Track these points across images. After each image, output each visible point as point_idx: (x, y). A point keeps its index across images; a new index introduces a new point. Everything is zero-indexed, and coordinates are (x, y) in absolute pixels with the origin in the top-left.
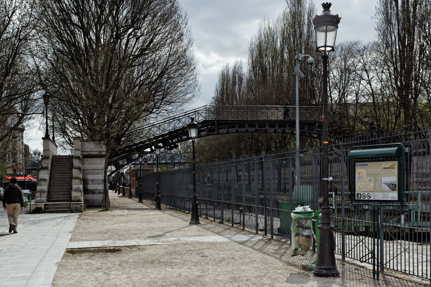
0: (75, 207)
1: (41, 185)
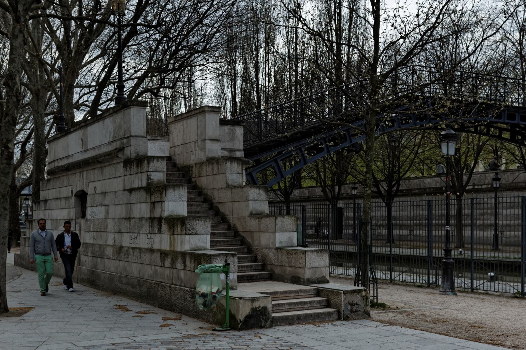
0: (351, 301)
1: (196, 234)
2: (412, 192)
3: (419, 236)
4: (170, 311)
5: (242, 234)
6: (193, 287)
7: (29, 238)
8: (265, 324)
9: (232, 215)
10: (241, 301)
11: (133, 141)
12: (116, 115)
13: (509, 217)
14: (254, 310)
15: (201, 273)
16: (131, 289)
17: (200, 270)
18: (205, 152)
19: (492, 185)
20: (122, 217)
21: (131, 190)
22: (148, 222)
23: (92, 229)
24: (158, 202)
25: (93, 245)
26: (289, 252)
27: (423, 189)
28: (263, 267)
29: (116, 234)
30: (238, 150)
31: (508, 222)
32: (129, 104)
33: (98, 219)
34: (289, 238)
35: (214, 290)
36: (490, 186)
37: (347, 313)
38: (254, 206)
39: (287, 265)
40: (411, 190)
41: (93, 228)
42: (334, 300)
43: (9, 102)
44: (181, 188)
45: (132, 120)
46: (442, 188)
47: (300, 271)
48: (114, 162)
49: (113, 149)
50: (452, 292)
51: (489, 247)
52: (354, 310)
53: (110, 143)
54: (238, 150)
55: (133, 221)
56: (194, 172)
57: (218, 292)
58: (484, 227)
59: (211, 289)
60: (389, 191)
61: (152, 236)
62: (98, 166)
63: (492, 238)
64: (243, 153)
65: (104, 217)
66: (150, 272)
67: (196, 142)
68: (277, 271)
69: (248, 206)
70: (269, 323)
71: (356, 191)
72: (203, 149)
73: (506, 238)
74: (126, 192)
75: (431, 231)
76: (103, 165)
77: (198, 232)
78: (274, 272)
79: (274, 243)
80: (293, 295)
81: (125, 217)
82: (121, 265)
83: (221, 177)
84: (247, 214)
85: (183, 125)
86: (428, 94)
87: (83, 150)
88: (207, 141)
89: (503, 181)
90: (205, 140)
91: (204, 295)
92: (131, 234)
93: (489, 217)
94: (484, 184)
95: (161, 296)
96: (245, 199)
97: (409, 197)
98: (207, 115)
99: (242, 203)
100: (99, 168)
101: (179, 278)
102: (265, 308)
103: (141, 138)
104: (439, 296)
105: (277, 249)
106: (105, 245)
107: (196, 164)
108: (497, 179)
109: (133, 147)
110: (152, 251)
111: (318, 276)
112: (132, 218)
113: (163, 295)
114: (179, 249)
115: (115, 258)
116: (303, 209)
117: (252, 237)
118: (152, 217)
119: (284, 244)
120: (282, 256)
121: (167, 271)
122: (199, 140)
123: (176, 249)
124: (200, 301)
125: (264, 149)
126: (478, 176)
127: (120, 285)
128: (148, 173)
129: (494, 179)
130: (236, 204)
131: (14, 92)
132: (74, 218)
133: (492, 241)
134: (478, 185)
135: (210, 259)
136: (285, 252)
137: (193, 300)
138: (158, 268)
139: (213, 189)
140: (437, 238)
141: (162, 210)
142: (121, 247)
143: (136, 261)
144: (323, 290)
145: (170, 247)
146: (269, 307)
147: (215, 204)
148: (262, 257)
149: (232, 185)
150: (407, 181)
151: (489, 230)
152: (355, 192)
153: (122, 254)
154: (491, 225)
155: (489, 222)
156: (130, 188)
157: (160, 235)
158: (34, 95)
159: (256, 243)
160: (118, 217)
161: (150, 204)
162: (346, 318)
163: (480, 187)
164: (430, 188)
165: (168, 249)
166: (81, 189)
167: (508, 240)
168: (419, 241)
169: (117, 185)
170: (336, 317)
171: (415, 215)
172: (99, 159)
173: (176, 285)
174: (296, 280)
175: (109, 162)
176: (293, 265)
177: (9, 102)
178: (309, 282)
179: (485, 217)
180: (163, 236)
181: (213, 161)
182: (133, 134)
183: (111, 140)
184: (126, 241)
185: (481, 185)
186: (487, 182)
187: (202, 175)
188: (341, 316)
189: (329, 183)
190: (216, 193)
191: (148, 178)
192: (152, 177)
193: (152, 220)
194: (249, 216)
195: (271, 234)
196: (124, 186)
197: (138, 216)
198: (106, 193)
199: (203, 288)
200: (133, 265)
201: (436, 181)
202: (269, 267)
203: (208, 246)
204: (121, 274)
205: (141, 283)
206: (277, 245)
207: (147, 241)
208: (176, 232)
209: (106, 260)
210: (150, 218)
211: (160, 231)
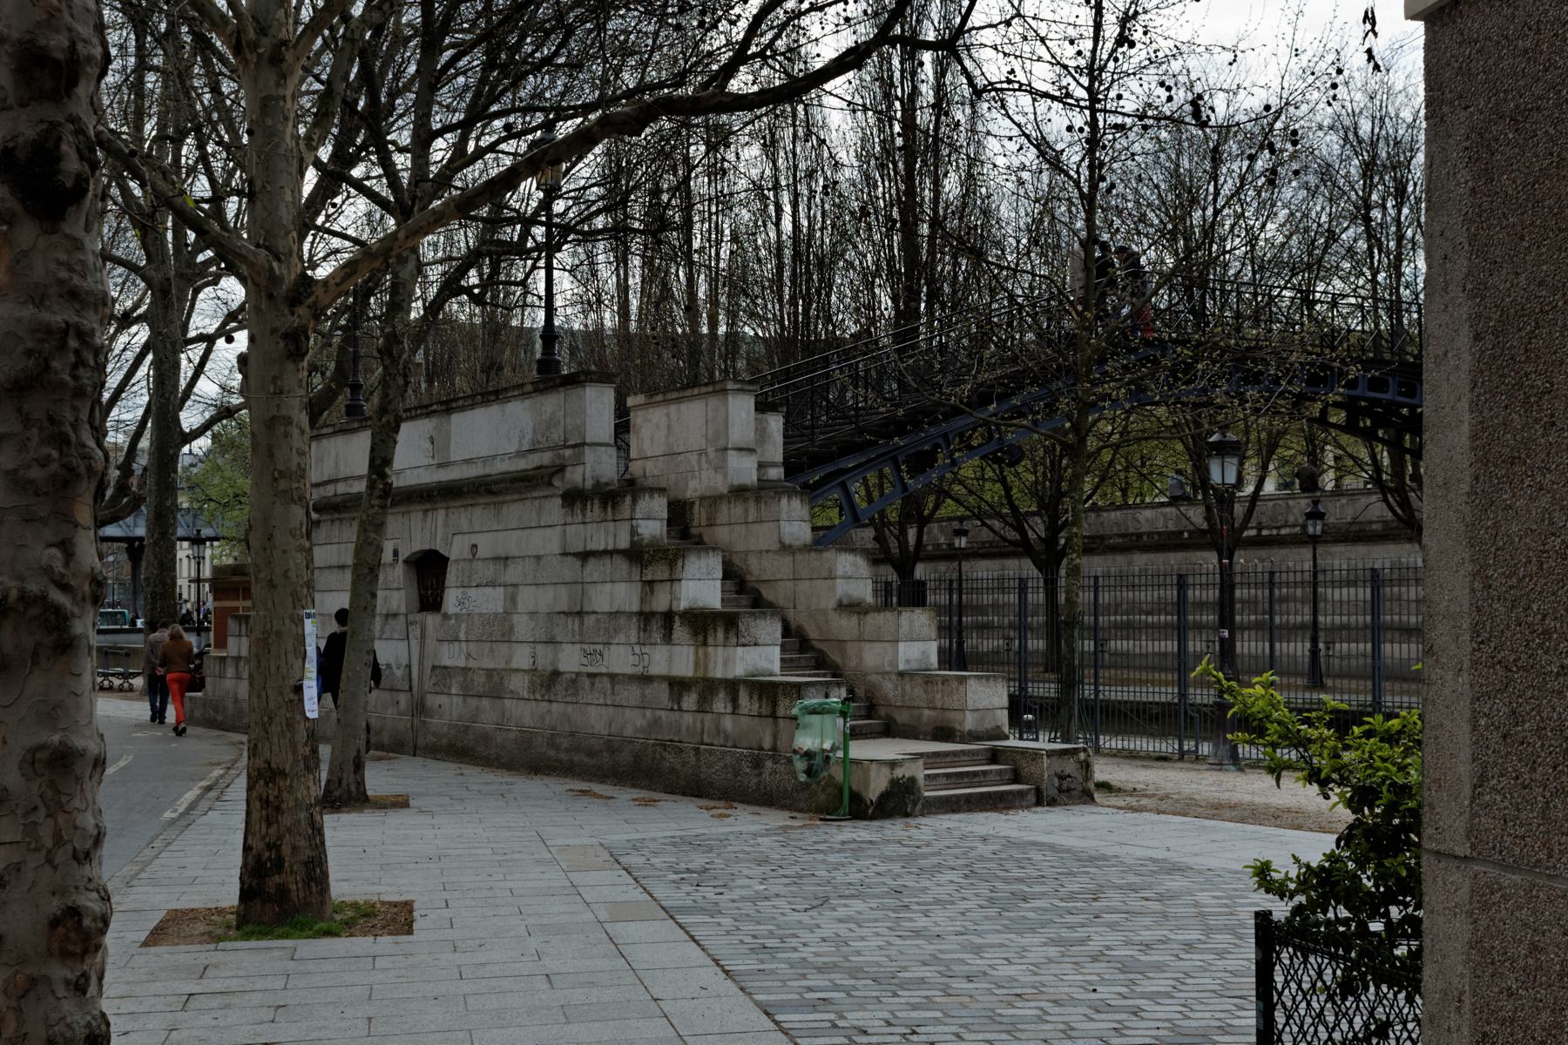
1: (756, 645)
2: (1106, 542)
3: (1127, 654)
4: (696, 796)
5: (818, 645)
6: (754, 745)
7: (238, 659)
8: (913, 810)
9: (795, 607)
10: (874, 766)
11: (589, 455)
12: (540, 398)
13: (1345, 606)
14: (894, 783)
15: (804, 714)
16: (586, 760)
17: (801, 709)
18: (725, 475)
19: (1304, 527)
20: (558, 610)
21: (585, 556)
22: (635, 620)
23: (462, 636)
24: (662, 581)
25: (466, 670)
26: (929, 680)
27: (1132, 534)
28: (871, 710)
29: (540, 648)
30: (774, 465)
31: (1345, 618)
32: (582, 377)
33: (481, 615)
34: (923, 652)
35: (827, 746)
37: (1053, 792)
38: (844, 589)
39: (922, 704)
40: (1102, 538)
41: (466, 633)
42: (1027, 768)
43: (389, 387)
44: (711, 554)
45: (588, 412)
46: (1181, 533)
48: (535, 494)
49: (530, 467)
50: (1234, 765)
51: (1300, 681)
52: (1065, 786)
53: (521, 454)
54: (774, 465)
55: (590, 621)
56: (696, 516)
57: (834, 749)
58: (1292, 631)
59: (822, 743)
60: (1051, 540)
61: (646, 649)
62: (482, 500)
63: (1307, 660)
64: (782, 470)
65: (501, 610)
66: (640, 722)
67: (702, 452)
68: (902, 717)
69: (833, 589)
70: (919, 807)
71: (964, 540)
72: (721, 467)
73: (1341, 658)
74: (570, 558)
75: (1186, 640)
76: (500, 498)
77: (760, 641)
78: (895, 721)
79: (894, 663)
80: (949, 759)
81: (566, 609)
82: (554, 710)
83: (766, 527)
84: (832, 604)
85: (668, 415)
86: (1414, 699)
87: (435, 462)
88: (731, 453)
89: (1331, 520)
90: (726, 449)
91: (809, 755)
92: (585, 647)
93: (1299, 606)
94: (1285, 526)
95: (673, 769)
96: (825, 574)
97: (1098, 554)
98: (730, 398)
99: (819, 583)
100: (486, 504)
101: (718, 730)
102: (912, 780)
103: (603, 449)
104: (1209, 773)
105: (901, 674)
106: (505, 670)
107: (702, 498)
108: (1315, 515)
109: (588, 466)
110: (645, 679)
111: (989, 727)
112: (588, 613)
113: (678, 766)
114: (718, 673)
115: (538, 696)
116: (886, 590)
117: (843, 652)
118: (647, 609)
119: (914, 666)
120: (912, 688)
121: (688, 719)
122: (710, 450)
123: (711, 674)
124: (800, 765)
125: (816, 460)
126: (1270, 504)
127: (552, 753)
128: (634, 522)
129: (1310, 516)
130: (804, 586)
131: (401, 366)
132: (403, 610)
133: (1307, 666)
134: (1271, 528)
135: (799, 692)
136: (920, 680)
137: (756, 772)
138: (663, 714)
139: (747, 553)
140: (1150, 658)
141: (674, 597)
142: (556, 674)
143: (602, 701)
144: (1003, 751)
145: (696, 670)
146: (921, 781)
147: (750, 584)
148: (867, 691)
149: (790, 546)
150: (1093, 515)
151: (1299, 639)
152: (962, 542)
153: (558, 687)
154: (1302, 627)
155: (1299, 618)
156: (581, 549)
157: (668, 647)
158: (158, 294)
159: (853, 663)
160: (543, 609)
162: (1052, 803)
163: (1275, 532)
164: (1150, 534)
165: (690, 673)
166: (426, 547)
167: (1345, 663)
168: (1128, 667)
169: (547, 542)
170: (1034, 800)
171: (1112, 602)
172: (494, 488)
173: (711, 745)
174: (943, 733)
175: (520, 493)
176: (939, 704)
177: (389, 387)
178: (973, 737)
179: (1292, 605)
180: (676, 649)
181: (748, 494)
182: (588, 440)
183: (526, 447)
184: (570, 660)
185: (1278, 528)
186: (1291, 519)
187: (719, 521)
188: (1041, 799)
189: (893, 516)
190: (753, 562)
192: (640, 531)
193: (645, 617)
194: (835, 610)
195: (887, 644)
196: (564, 547)
197: (607, 609)
199: (806, 742)
200: (592, 709)
201: (1165, 515)
202: (883, 712)
204: (553, 729)
206: (901, 667)
207: (632, 659)
208: (710, 640)
209: (508, 703)
210: (640, 614)
211: (668, 638)
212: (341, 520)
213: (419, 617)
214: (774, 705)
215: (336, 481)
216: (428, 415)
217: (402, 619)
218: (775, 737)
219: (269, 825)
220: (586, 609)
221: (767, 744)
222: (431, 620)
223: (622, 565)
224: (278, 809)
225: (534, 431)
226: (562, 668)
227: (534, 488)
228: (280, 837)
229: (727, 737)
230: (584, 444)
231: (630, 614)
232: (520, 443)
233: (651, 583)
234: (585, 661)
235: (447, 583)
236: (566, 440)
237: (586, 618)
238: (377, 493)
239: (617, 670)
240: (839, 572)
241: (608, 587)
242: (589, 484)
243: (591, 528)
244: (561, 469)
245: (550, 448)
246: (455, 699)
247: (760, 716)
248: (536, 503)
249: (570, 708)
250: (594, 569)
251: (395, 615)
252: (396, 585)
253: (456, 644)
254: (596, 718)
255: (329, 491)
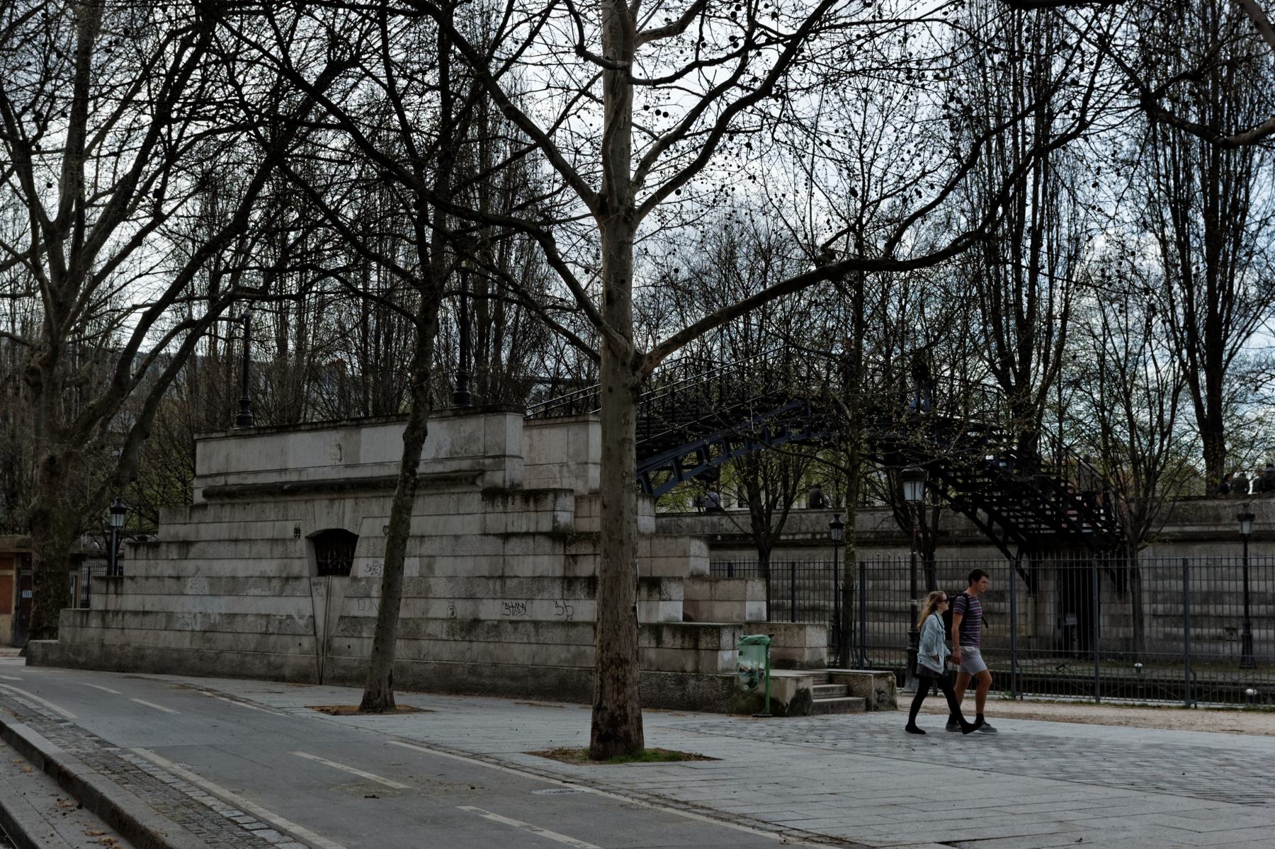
14: (798, 692)
16: (509, 683)
18: (586, 482)
19: (829, 533)
21: (506, 536)
36: (809, 536)
42: (856, 685)
47: (797, 651)
61: (571, 603)
69: (688, 564)
87: (343, 462)
90: (586, 463)
94: (800, 532)
110: (570, 624)
118: (570, 574)
119: (754, 618)
143: (525, 640)
156: (502, 530)
161: (563, 558)
162: (877, 709)
183: (442, 455)
184: (491, 610)
186: (804, 528)
191: (555, 520)
198: (423, 537)
201: (702, 522)
203: (681, 618)
205: (534, 672)
206: (748, 618)
209: (424, 643)
210: (564, 578)
212: (233, 505)
213: (322, 579)
214: (697, 640)
215: (227, 474)
216: (335, 428)
217: (305, 582)
218: (697, 663)
219: (619, 694)
220: (507, 574)
221: (689, 667)
222: (337, 582)
223: (546, 544)
224: (624, 684)
225: (453, 445)
226: (482, 616)
227: (455, 485)
228: (626, 702)
229: (651, 664)
230: (504, 456)
231: (554, 579)
232: (437, 451)
233: (574, 556)
234: (507, 612)
235: (356, 554)
236: (485, 452)
237: (508, 582)
238: (410, 486)
239: (540, 618)
240: (692, 553)
241: (531, 559)
242: (508, 484)
243: (510, 517)
244: (482, 473)
245: (471, 458)
246: (366, 641)
247: (683, 649)
248: (455, 497)
249: (491, 646)
250: (514, 546)
251: (297, 578)
252: (298, 555)
253: (367, 600)
254: (519, 652)
255: (220, 481)
